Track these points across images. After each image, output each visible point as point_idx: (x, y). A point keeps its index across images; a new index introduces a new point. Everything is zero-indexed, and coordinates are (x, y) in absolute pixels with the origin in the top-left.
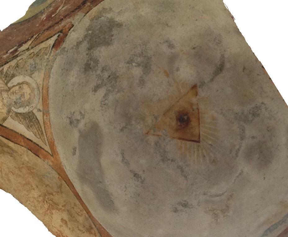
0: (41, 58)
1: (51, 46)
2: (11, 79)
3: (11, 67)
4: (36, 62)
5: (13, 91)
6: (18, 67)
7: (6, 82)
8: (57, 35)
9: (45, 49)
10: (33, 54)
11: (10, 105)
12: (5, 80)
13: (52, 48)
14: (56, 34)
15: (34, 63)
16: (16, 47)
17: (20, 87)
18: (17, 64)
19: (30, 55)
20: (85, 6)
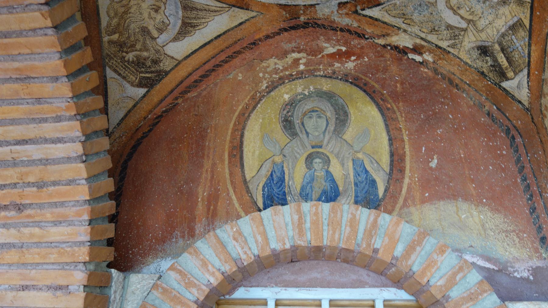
0: (403, 8)
1: (380, 7)
2: (455, 27)
3: (440, 37)
4: (412, 9)
5: (470, 14)
6: (434, 29)
7: (462, 33)
8: (364, 12)
9: (389, 12)
10: (405, 22)
11: (493, 7)
12: (460, 34)
13: (382, 4)
14: (364, 16)
15: (417, 11)
16: (411, 56)
17: (459, 8)
18: (432, 31)
19: (409, 24)
20: (308, 19)
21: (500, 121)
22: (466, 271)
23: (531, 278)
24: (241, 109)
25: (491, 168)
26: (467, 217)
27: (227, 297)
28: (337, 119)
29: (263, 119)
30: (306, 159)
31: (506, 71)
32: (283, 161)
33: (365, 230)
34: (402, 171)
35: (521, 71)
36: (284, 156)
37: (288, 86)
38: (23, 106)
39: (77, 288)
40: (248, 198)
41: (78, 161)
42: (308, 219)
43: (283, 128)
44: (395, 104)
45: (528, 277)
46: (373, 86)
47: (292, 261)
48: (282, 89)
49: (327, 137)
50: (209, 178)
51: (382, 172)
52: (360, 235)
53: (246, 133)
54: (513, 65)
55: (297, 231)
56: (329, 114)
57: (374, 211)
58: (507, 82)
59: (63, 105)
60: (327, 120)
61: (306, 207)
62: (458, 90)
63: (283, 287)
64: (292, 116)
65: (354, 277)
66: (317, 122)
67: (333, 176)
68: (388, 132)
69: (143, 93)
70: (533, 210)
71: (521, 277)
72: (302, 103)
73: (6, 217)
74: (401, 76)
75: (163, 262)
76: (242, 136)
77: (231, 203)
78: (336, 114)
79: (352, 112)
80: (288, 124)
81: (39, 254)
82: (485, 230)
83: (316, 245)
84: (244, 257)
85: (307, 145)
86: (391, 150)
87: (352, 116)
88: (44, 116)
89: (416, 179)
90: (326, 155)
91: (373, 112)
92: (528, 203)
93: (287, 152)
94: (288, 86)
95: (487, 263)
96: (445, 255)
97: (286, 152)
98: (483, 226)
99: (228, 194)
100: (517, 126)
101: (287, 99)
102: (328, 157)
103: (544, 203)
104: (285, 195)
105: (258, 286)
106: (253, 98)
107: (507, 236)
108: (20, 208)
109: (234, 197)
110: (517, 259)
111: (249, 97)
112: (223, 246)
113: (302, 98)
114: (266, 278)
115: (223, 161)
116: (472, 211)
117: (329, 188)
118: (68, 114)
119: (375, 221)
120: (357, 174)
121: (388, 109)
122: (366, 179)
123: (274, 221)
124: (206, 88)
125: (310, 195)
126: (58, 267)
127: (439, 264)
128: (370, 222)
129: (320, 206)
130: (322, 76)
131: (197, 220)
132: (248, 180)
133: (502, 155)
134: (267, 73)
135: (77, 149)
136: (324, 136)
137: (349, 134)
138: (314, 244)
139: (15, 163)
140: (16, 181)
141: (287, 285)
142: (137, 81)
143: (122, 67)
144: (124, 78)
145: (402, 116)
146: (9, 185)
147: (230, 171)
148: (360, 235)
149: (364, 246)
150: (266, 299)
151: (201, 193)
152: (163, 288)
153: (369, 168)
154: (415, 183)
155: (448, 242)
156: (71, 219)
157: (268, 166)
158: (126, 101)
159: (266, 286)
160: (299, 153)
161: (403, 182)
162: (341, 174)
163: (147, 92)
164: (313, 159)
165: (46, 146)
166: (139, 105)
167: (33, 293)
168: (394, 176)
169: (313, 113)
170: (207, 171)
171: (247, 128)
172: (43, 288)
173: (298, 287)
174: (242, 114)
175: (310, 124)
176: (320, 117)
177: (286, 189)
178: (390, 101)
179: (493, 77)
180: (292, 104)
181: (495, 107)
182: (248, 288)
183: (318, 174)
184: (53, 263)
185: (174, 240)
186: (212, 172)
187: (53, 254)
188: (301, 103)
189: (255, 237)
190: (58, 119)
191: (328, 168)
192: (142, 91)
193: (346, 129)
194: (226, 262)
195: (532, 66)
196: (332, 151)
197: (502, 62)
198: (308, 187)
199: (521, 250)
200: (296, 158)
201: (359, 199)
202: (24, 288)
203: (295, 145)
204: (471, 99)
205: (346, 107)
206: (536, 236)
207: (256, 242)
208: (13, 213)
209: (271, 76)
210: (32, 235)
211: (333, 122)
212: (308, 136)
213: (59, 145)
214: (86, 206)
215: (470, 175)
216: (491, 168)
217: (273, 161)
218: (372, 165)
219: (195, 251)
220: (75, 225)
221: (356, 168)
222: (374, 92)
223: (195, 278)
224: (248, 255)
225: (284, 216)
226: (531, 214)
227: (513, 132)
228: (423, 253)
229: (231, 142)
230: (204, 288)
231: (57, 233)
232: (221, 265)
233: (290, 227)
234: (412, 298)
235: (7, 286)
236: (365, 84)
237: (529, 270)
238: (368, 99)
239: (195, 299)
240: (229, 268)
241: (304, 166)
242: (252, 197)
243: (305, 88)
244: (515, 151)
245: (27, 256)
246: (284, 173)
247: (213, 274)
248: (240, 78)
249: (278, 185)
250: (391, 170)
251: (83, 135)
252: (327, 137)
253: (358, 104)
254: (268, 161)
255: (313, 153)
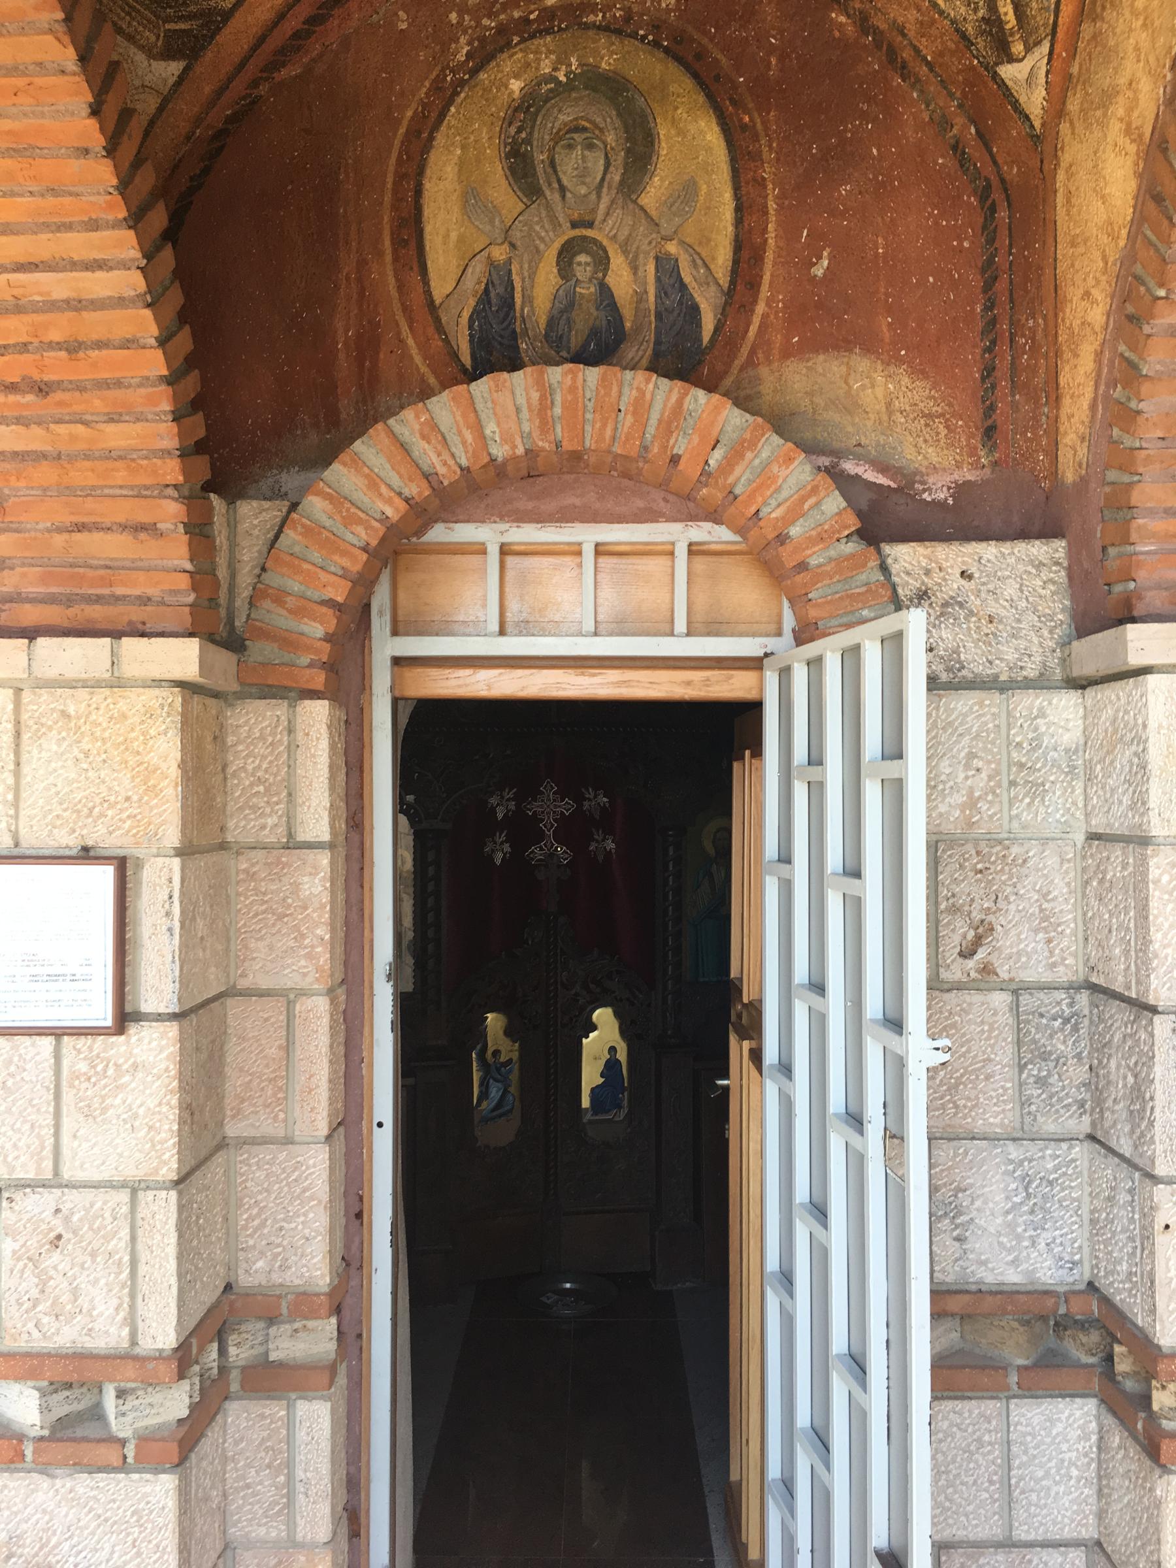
21: (975, 165)
22: (822, 494)
23: (950, 501)
24: (412, 118)
25: (931, 279)
26: (863, 387)
27: (414, 539)
28: (628, 151)
29: (463, 148)
30: (560, 254)
31: (1010, 39)
32: (510, 258)
33: (660, 421)
34: (754, 286)
35: (1038, 43)
36: (513, 246)
37: (520, 55)
38: (24, 200)
39: (173, 527)
40: (440, 343)
41: (140, 304)
42: (558, 398)
43: (508, 173)
44: (760, 115)
45: (946, 499)
46: (716, 60)
47: (529, 476)
48: (507, 63)
49: (605, 201)
50: (355, 296)
51: (713, 288)
52: (651, 430)
53: (427, 185)
54: (1025, 26)
55: (537, 422)
56: (610, 138)
57: (679, 383)
58: (1009, 66)
59: (102, 199)
60: (606, 155)
61: (556, 374)
62: (904, 81)
63: (513, 521)
64: (528, 141)
65: (640, 503)
66: (584, 158)
67: (612, 295)
68: (736, 188)
69: (177, 73)
70: (989, 371)
71: (933, 500)
72: (553, 107)
73: (19, 405)
74: (782, 35)
75: (284, 476)
76: (418, 192)
77: (406, 356)
78: (627, 140)
79: (662, 132)
80: (521, 168)
81: (93, 470)
82: (890, 413)
83: (570, 448)
84: (442, 470)
85: (561, 219)
86: (737, 236)
87: (663, 144)
88: (67, 220)
89: (780, 305)
90: (601, 244)
91: (710, 135)
92: (982, 356)
93: (518, 234)
94: (520, 55)
95: (880, 476)
96: (792, 467)
97: (516, 235)
98: (889, 404)
99: (399, 333)
100: (1008, 178)
101: (517, 95)
102: (606, 252)
103: (1013, 358)
104: (516, 339)
105: (468, 521)
106: (437, 86)
107: (927, 425)
108: (43, 389)
109: (410, 342)
110: (935, 468)
111: (427, 84)
112: (404, 448)
113: (551, 90)
114: (483, 506)
115: (380, 254)
116: (875, 375)
117: (604, 323)
118: (110, 217)
119: (680, 402)
120: (662, 292)
121: (744, 127)
122: (680, 303)
123: (493, 402)
124: (321, 55)
125: (565, 339)
126: (131, 493)
127: (780, 481)
128: (669, 405)
129: (581, 374)
130: (599, 28)
131: (339, 391)
132: (437, 302)
133: (961, 250)
134: (468, 12)
135: (134, 282)
136: (599, 197)
137: (653, 194)
138: (567, 446)
139: (19, 308)
140: (24, 338)
141: (521, 517)
142: (159, 44)
143: (123, 10)
144: (130, 38)
145: (770, 146)
146: (14, 346)
147: (397, 280)
148: (651, 430)
149: (656, 450)
150: (484, 544)
151: (340, 331)
152: (304, 526)
153: (687, 279)
154: (777, 313)
155: (819, 437)
156: (140, 409)
157: (478, 270)
158: (142, 96)
159: (483, 522)
160: (542, 239)
161: (752, 311)
162: (631, 291)
163: (186, 70)
164: (574, 255)
165: (74, 274)
166: (170, 106)
167: (97, 536)
168: (736, 298)
169: (575, 136)
170: (348, 278)
171: (428, 172)
172: (114, 528)
173: (541, 522)
174: (414, 133)
175: (570, 163)
176: (590, 147)
177: (518, 323)
178: (751, 105)
179: (985, 47)
180: (528, 108)
181: (973, 130)
182: (451, 525)
183: (583, 291)
184: (121, 487)
185: (299, 432)
186: (359, 280)
187: (118, 470)
188: (549, 105)
189: (460, 433)
190: (93, 225)
191: (604, 276)
192: (174, 68)
193: (647, 179)
194: (411, 480)
195: (1060, 34)
196: (615, 236)
197: (1006, 14)
198: (562, 322)
199: (946, 452)
200: (538, 251)
201: (663, 348)
202: (80, 528)
203: (536, 219)
204: (928, 106)
205: (650, 118)
206: (979, 424)
207: (464, 443)
208: (30, 398)
209: (478, 23)
210: (73, 438)
211: (619, 158)
212: (563, 197)
213: (100, 274)
214: (163, 387)
215: (887, 295)
216: (931, 279)
217: (489, 257)
218: (695, 273)
219: (353, 461)
220: (147, 421)
221: (663, 278)
222: (717, 78)
223: (359, 509)
224: (449, 466)
225: (513, 393)
226: (983, 379)
227: (997, 195)
228: (757, 462)
229: (394, 208)
230: (376, 524)
231: (118, 436)
232: (402, 485)
233: (525, 414)
234: (738, 538)
235: (49, 525)
236: (699, 56)
237: (949, 488)
238: (702, 98)
239: (362, 544)
240: (416, 489)
241: (555, 270)
242: (447, 341)
243: (559, 61)
244: (987, 242)
245: (71, 474)
246: (513, 288)
247: (389, 501)
248: (404, 26)
249: (501, 315)
250: (733, 282)
251: (144, 257)
252: (605, 201)
253: (679, 111)
254: (478, 257)
255: (573, 239)
